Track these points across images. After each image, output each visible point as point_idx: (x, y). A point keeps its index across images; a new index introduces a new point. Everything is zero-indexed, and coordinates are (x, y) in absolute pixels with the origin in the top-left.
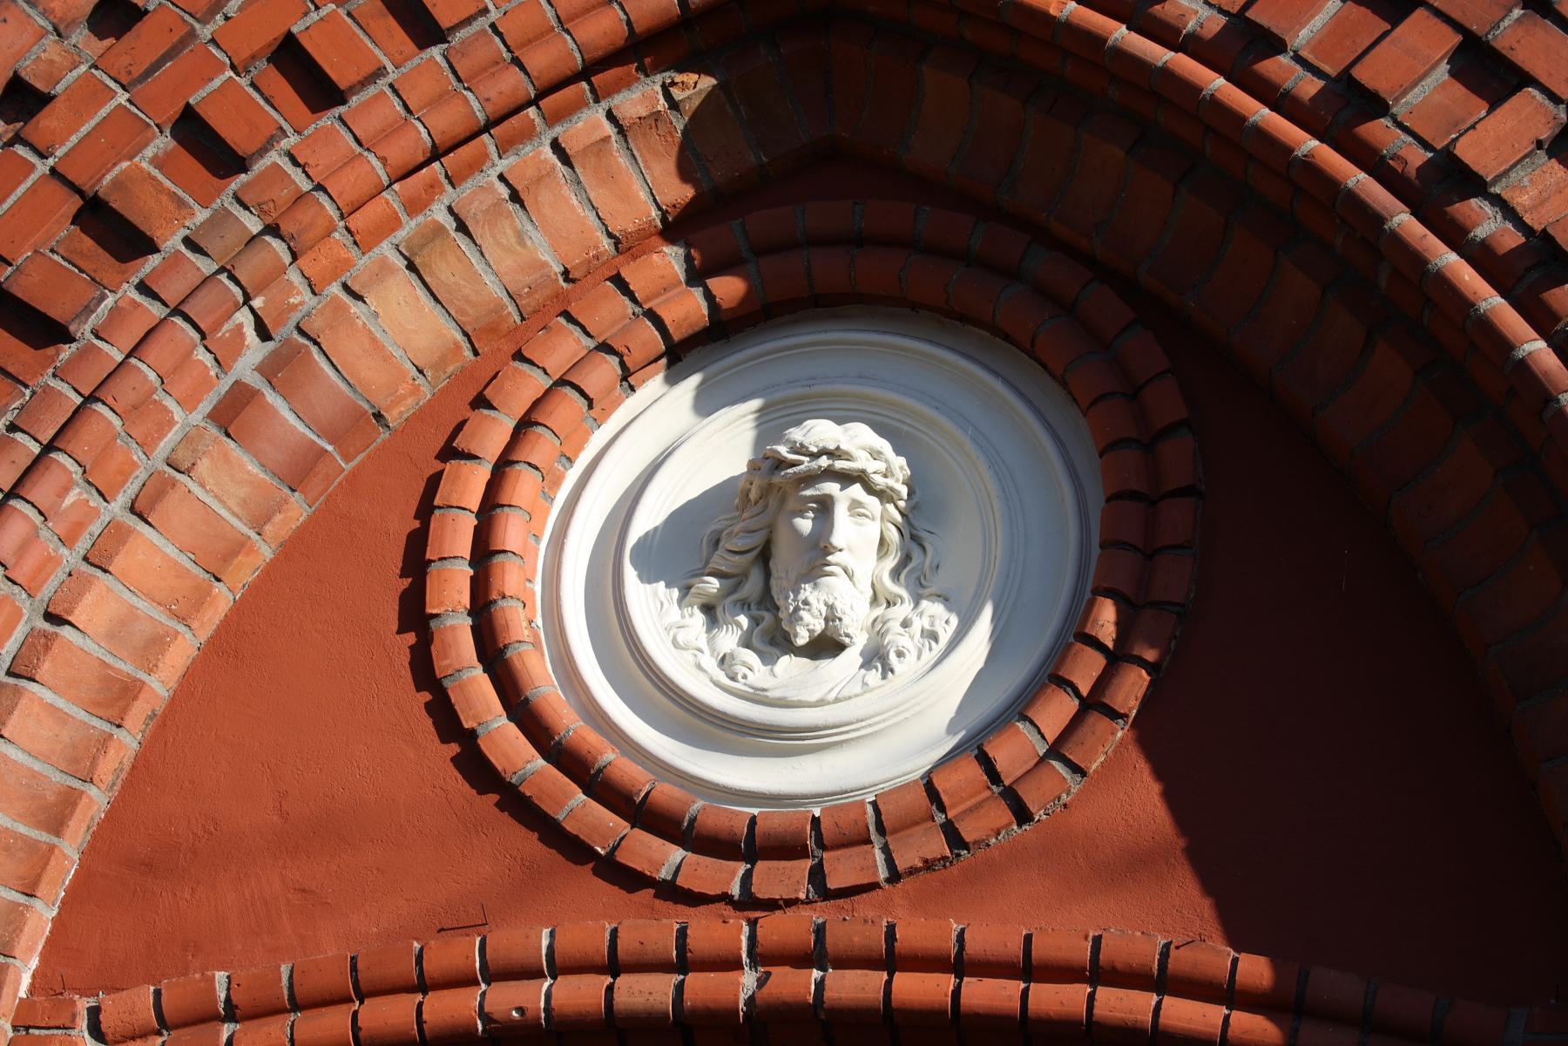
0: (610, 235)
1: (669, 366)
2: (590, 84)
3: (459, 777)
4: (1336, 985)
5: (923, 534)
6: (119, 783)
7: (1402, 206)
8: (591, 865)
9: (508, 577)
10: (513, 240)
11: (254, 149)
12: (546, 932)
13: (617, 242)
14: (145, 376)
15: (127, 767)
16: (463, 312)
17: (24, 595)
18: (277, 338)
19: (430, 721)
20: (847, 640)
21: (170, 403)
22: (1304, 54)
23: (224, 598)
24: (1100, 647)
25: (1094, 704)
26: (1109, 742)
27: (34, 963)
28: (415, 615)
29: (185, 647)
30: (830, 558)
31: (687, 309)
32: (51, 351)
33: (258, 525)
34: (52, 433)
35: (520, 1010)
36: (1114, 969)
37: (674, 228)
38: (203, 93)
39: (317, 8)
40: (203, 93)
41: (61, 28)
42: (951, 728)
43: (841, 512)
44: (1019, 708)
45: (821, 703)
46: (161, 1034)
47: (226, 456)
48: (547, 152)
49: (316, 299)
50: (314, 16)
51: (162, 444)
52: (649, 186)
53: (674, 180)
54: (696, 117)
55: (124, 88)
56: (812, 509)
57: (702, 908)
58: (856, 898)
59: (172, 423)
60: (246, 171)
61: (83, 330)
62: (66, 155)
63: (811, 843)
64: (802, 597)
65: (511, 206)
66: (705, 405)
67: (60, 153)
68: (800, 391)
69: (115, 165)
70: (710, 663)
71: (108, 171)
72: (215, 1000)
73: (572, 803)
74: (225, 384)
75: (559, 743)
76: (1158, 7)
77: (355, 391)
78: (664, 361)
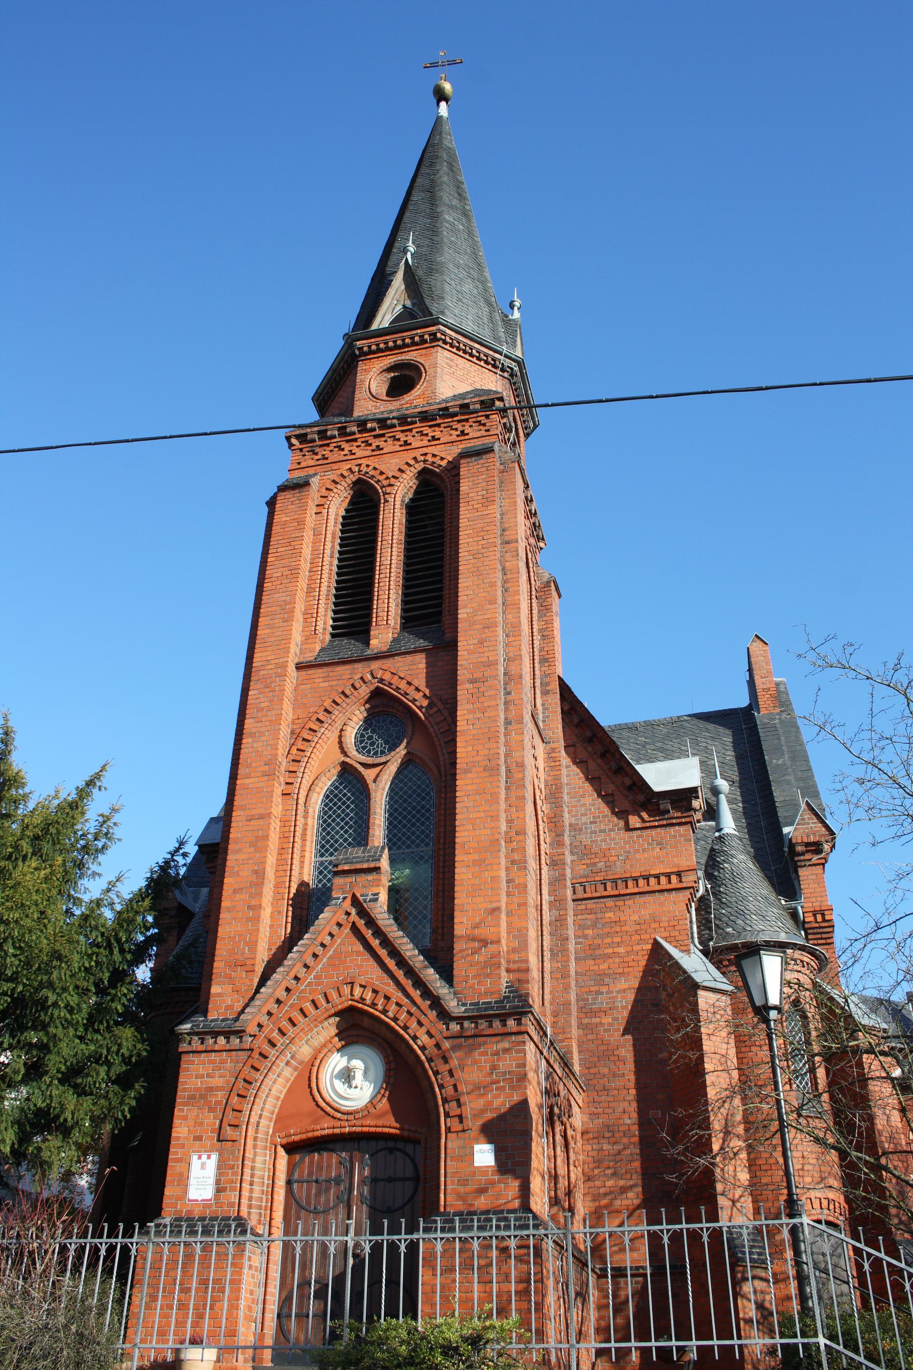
4: (406, 1127)
9: (320, 1081)
23: (289, 1085)
25: (383, 1096)
26: (385, 1100)
28: (310, 1086)
29: (285, 1091)
31: (339, 1045)
37: (336, 1035)
44: (376, 1096)
52: (334, 1031)
66: (342, 1056)
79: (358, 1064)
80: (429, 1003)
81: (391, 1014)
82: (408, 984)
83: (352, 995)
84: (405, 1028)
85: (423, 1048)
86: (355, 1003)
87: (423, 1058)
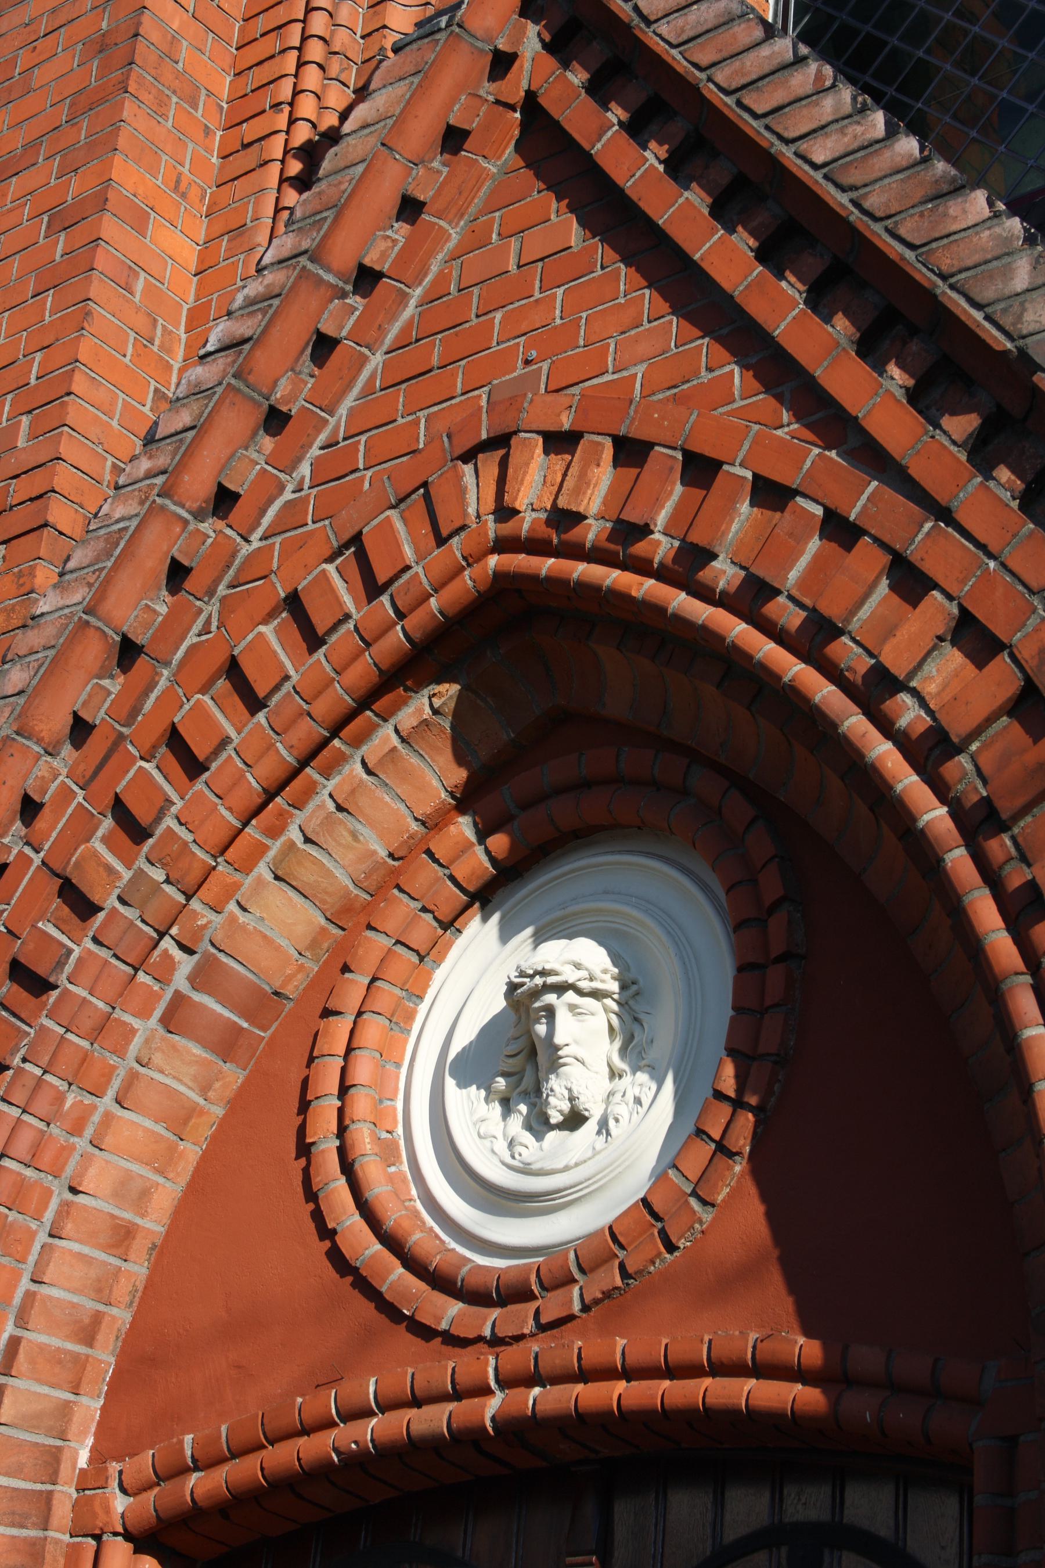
0: (416, 819)
1: (483, 907)
2: (372, 711)
3: (330, 1266)
4: (867, 1358)
5: (642, 1016)
6: (137, 1300)
7: (855, 709)
8: (405, 1324)
10: (350, 839)
11: (151, 820)
12: (373, 1380)
13: (423, 823)
14: (96, 1006)
15: (141, 1288)
16: (324, 902)
17: (50, 1178)
18: (199, 951)
19: (313, 1225)
20: (586, 1114)
21: (127, 1018)
22: (795, 593)
23: (191, 1152)
24: (727, 1098)
27: (90, 1441)
29: (168, 1191)
30: (560, 1053)
31: (477, 863)
32: (44, 998)
33: (204, 1090)
34: (47, 1058)
35: (356, 1442)
36: (722, 1363)
37: (465, 801)
38: (124, 783)
39: (188, 700)
40: (124, 783)
41: (50, 750)
42: (650, 1179)
43: (562, 1016)
45: (566, 1169)
46: (159, 1485)
47: (174, 1047)
48: (358, 768)
49: (221, 916)
50: (187, 707)
51: (131, 1047)
52: (438, 776)
53: (453, 766)
54: (457, 714)
55: (81, 788)
56: (543, 1016)
57: (470, 1349)
58: (563, 1328)
59: (133, 1032)
60: (151, 836)
61: (63, 980)
62: (50, 848)
63: (535, 1288)
64: (549, 1086)
65: (340, 815)
67: (46, 847)
68: (559, 914)
69: (76, 849)
70: (501, 1146)
71: (72, 855)
72: (222, 1450)
73: (393, 1277)
74: (168, 995)
75: (386, 1231)
76: (701, 573)
77: (259, 978)
78: (477, 905)
79: (582, 958)
80: (962, 425)
81: (724, 573)
82: (824, 344)
83: (505, 512)
84: (815, 638)
85: (930, 751)
86: (521, 562)
87: (934, 815)
